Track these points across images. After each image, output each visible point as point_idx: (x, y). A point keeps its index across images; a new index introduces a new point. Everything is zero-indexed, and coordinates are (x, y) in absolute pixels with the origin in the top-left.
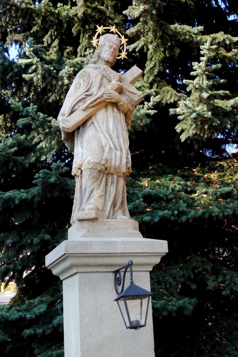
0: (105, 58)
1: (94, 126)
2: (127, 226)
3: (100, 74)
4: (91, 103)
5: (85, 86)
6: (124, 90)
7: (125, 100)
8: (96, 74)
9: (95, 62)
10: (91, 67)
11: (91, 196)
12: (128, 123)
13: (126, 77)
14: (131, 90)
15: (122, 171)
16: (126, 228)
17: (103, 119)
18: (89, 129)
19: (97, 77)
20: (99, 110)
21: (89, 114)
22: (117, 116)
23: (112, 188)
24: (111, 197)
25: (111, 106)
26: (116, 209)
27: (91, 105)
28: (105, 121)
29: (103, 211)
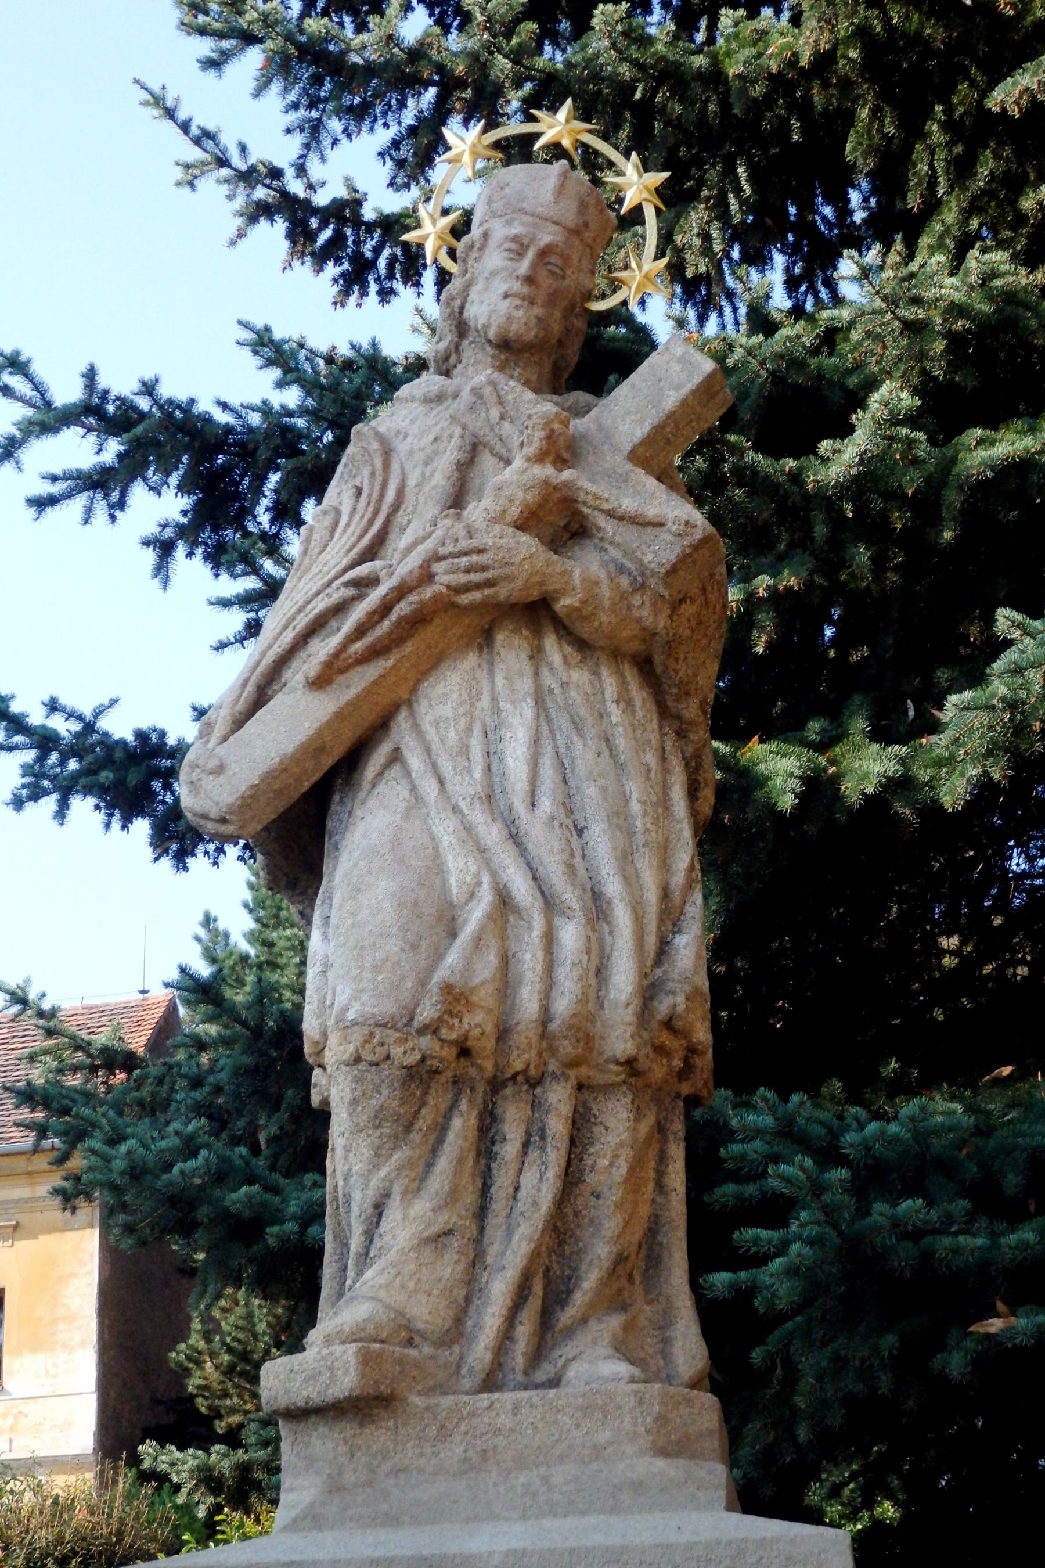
0: (486, 327)
1: (408, 774)
2: (604, 1436)
3: (458, 431)
4: (360, 631)
5: (356, 528)
6: (586, 510)
7: (602, 574)
8: (431, 437)
9: (447, 359)
10: (413, 399)
11: (378, 1243)
12: (679, 717)
13: (607, 421)
14: (628, 504)
15: (609, 1053)
16: (595, 1446)
17: (463, 723)
18: (371, 803)
19: (436, 453)
20: (432, 664)
21: (354, 705)
22: (564, 685)
23: (529, 1179)
24: (516, 1238)
25: (517, 631)
26: (566, 1316)
27: (359, 646)
28: (477, 730)
29: (456, 1332)
